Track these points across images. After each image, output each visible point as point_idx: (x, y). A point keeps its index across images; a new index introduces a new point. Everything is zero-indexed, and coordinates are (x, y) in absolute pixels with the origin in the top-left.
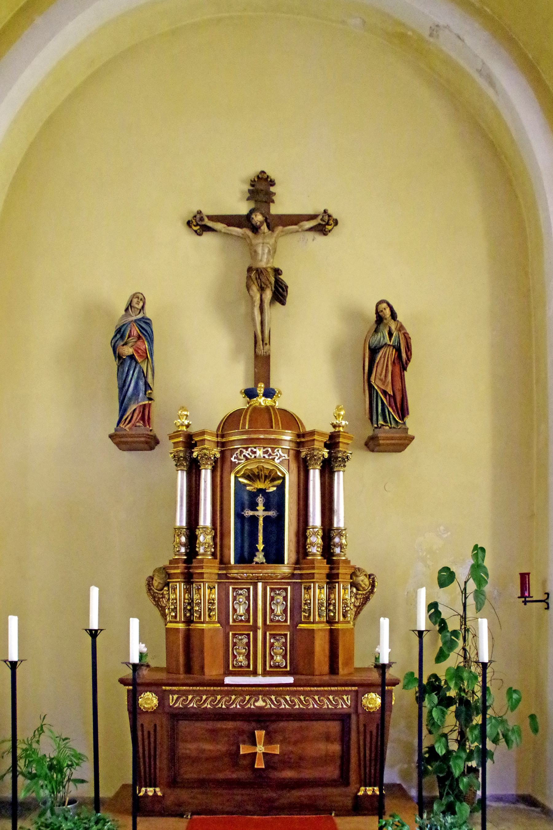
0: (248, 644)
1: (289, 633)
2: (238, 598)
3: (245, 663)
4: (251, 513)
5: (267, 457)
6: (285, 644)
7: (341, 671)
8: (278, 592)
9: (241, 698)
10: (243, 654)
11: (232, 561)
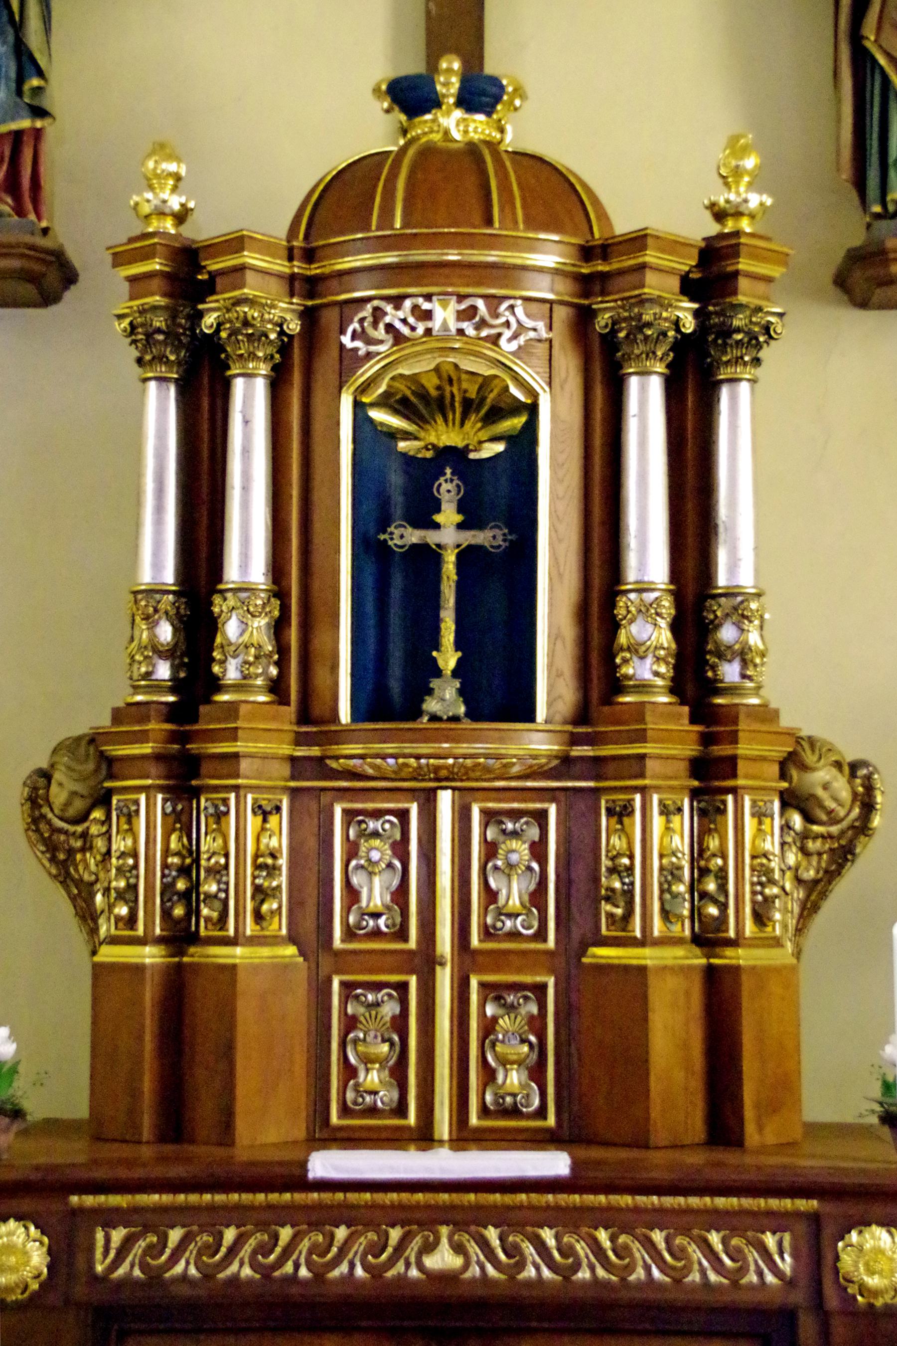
0: (400, 1023)
1: (551, 981)
2: (364, 846)
3: (387, 1096)
4: (414, 536)
5: (470, 331)
6: (537, 1024)
7: (752, 1134)
8: (510, 826)
9: (372, 1236)
10: (383, 1062)
11: (345, 713)
